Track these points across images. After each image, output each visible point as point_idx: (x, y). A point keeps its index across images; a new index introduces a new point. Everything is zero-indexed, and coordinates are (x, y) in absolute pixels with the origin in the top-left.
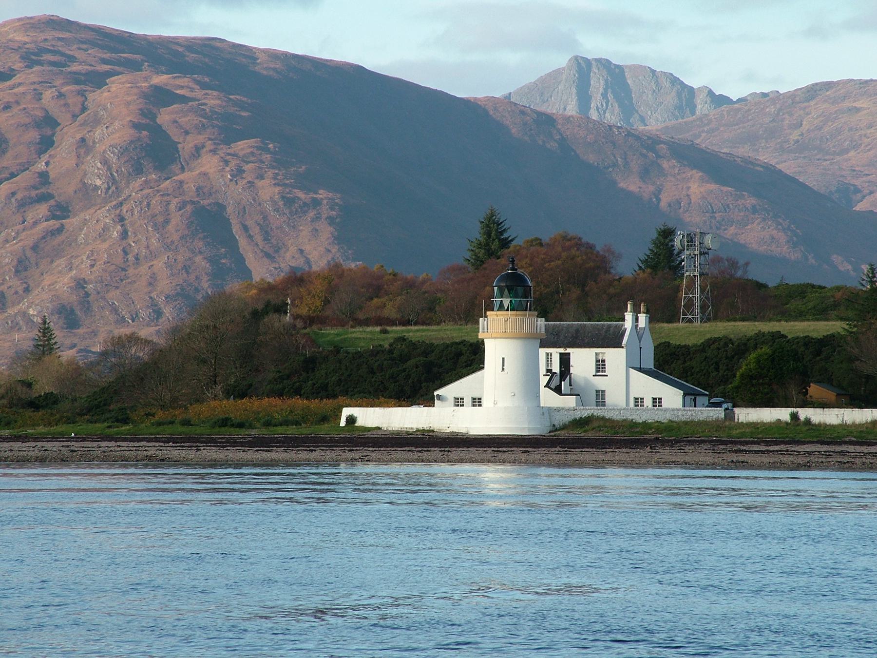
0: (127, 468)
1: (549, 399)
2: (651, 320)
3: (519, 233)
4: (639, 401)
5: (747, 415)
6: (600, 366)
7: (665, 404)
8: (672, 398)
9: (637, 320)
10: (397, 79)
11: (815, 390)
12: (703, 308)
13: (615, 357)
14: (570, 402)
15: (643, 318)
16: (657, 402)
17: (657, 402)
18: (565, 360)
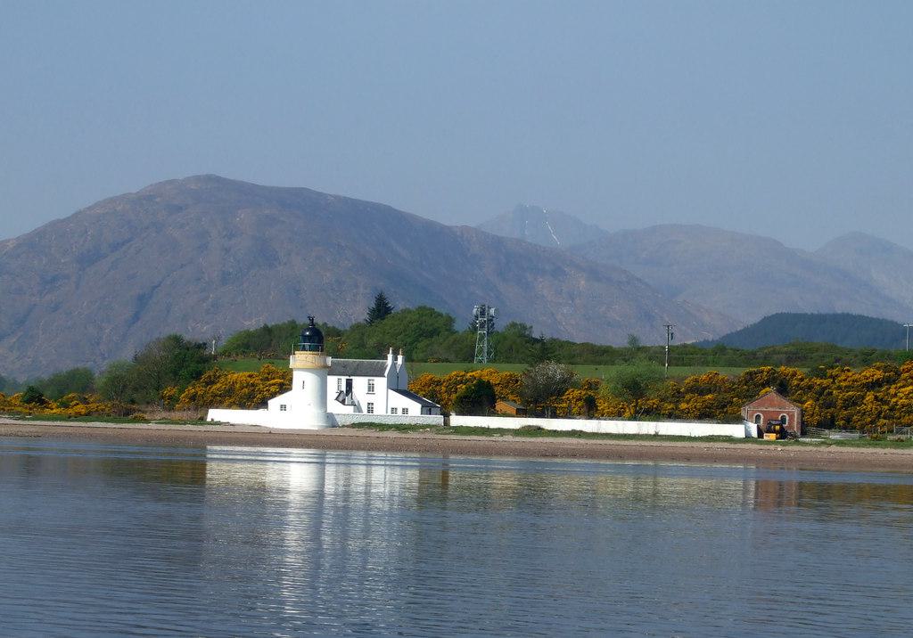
0: (406, 433)
1: (334, 407)
2: (408, 359)
3: (398, 304)
4: (394, 410)
5: (457, 420)
6: (371, 388)
7: (410, 413)
8: (415, 408)
9: (396, 359)
10: (377, 208)
11: (500, 405)
12: (489, 353)
13: (381, 383)
14: (350, 410)
15: (400, 358)
16: (405, 411)
17: (405, 411)
18: (349, 384)
